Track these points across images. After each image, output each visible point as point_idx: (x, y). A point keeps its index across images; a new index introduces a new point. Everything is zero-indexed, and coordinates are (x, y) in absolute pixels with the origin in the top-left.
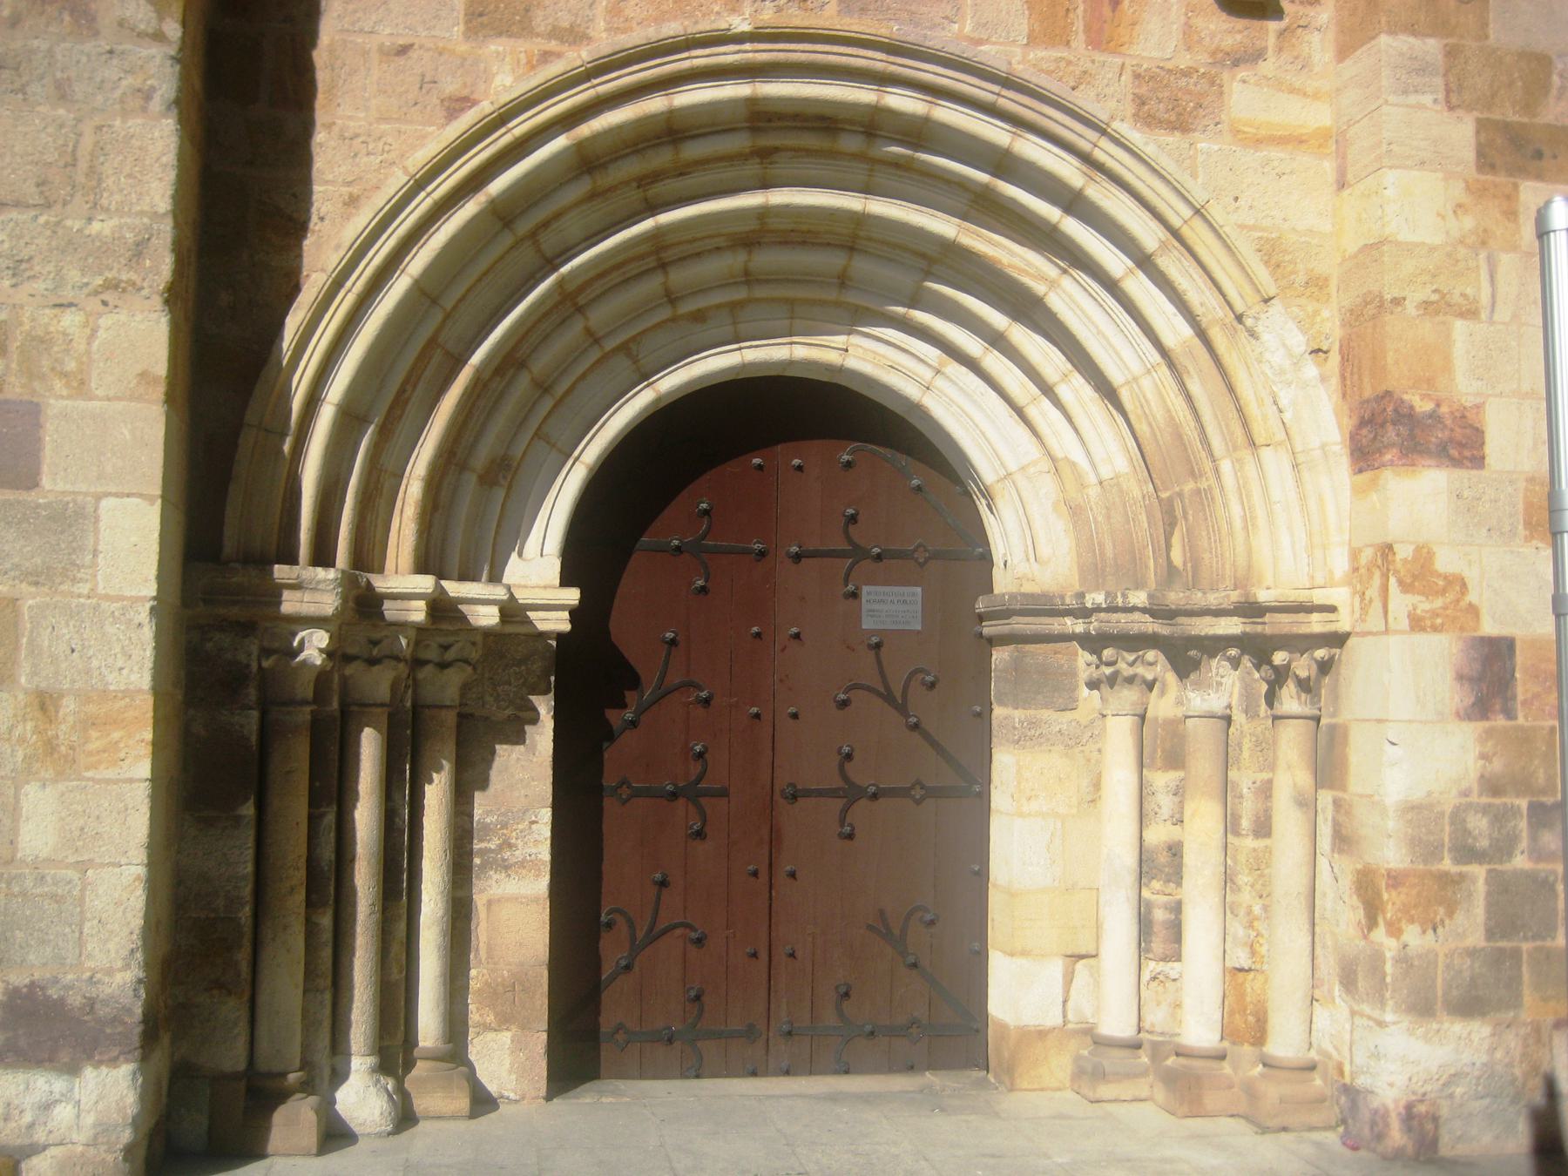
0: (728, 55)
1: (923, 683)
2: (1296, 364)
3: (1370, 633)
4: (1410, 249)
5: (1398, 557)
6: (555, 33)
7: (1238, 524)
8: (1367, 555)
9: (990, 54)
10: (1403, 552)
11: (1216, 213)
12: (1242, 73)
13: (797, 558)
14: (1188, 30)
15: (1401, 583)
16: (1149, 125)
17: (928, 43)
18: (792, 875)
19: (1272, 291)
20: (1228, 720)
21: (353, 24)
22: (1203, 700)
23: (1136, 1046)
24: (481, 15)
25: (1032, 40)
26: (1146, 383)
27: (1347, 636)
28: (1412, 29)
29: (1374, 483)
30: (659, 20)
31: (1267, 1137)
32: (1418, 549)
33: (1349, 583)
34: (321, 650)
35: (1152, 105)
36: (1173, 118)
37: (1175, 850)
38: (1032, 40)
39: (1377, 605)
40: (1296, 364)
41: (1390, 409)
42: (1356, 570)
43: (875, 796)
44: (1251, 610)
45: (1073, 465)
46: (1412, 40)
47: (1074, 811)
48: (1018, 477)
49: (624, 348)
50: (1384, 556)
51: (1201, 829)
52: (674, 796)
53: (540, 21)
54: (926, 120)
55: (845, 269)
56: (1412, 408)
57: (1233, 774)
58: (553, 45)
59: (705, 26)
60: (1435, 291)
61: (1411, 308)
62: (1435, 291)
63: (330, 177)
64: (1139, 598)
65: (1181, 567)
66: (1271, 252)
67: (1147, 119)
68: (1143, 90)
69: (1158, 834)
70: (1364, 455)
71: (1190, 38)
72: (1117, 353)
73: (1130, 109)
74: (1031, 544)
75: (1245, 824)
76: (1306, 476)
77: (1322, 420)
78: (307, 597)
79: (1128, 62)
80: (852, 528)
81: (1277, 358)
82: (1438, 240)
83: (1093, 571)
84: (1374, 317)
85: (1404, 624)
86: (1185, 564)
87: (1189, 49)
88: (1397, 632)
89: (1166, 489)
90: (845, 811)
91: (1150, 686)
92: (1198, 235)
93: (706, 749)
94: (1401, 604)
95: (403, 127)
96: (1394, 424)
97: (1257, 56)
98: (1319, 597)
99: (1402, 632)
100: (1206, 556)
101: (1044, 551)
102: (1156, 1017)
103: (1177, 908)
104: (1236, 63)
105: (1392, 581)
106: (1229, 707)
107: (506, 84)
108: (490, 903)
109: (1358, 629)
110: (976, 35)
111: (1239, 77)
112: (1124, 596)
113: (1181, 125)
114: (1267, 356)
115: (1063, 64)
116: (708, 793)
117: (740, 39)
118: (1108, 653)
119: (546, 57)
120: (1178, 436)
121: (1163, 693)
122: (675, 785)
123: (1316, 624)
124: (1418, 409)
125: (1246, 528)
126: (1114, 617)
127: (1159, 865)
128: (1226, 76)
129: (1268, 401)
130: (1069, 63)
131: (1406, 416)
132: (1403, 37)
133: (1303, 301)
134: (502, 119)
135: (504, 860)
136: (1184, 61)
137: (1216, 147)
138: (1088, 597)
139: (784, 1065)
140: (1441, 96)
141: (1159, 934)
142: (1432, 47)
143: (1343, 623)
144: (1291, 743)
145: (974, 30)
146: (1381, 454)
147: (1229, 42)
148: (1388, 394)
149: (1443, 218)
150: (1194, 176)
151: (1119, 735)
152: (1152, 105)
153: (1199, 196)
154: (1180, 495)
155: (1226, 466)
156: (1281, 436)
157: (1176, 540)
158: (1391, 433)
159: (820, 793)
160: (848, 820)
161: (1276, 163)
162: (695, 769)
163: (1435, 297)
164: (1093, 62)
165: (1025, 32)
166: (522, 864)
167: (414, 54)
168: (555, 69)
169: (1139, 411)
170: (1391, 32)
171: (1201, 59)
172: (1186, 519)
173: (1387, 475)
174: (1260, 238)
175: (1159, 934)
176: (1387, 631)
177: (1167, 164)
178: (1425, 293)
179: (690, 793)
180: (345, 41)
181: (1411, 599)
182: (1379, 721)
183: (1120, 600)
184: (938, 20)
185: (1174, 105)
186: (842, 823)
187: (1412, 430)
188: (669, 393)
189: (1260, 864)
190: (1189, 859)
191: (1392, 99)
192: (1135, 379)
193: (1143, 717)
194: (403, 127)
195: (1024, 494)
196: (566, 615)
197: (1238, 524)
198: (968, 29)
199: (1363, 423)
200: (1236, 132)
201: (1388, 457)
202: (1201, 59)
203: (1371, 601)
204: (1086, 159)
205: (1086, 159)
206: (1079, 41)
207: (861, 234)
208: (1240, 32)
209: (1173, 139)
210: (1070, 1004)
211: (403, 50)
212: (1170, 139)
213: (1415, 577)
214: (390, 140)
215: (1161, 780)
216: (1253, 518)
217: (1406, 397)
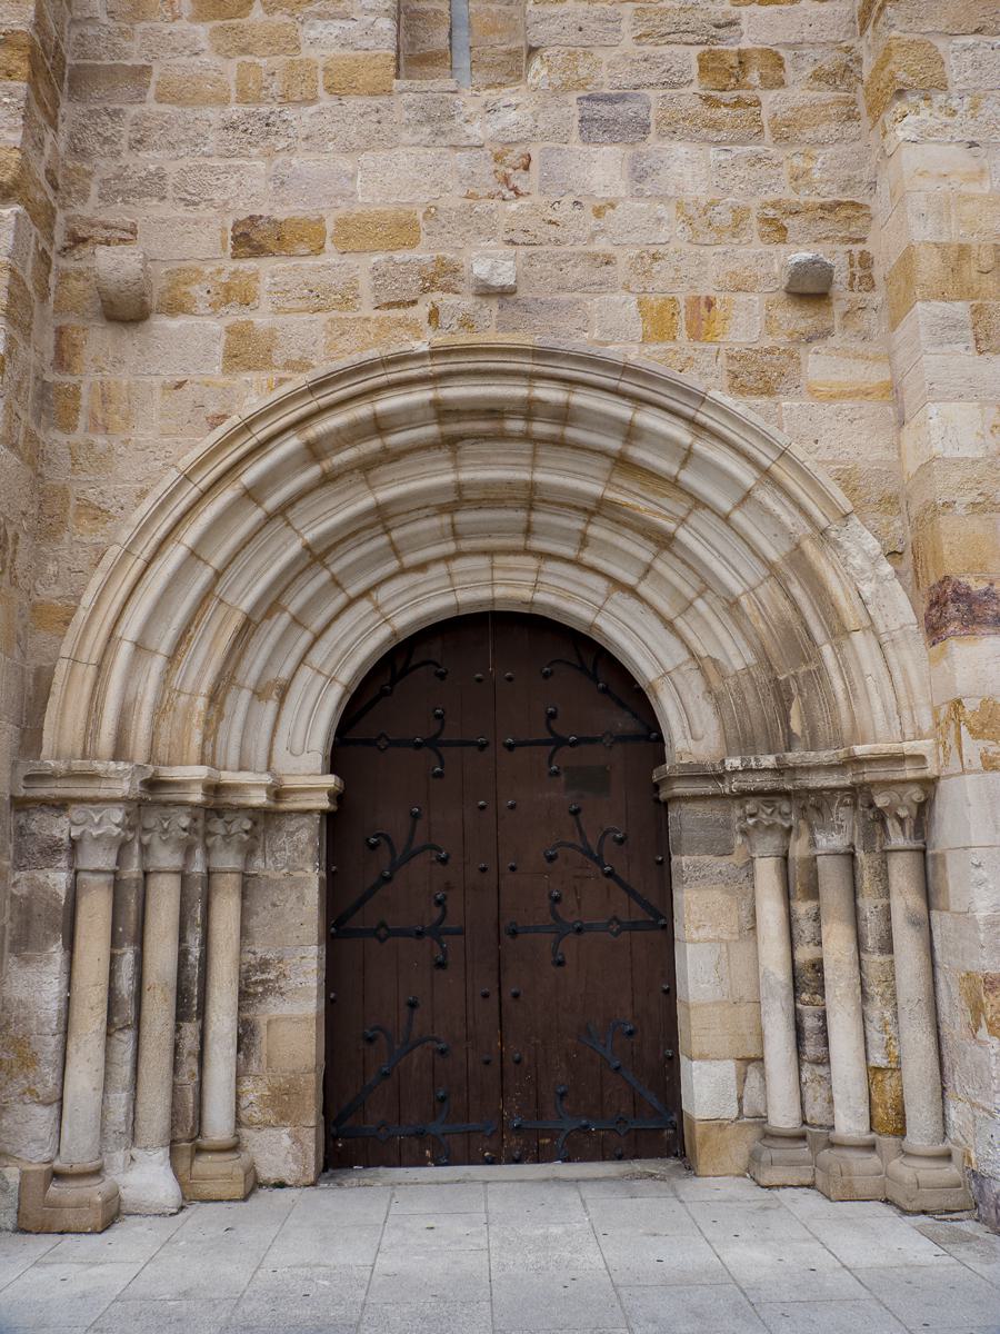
0: (413, 370)
1: (615, 839)
2: (874, 563)
3: (952, 775)
4: (956, 463)
6: (288, 365)
7: (841, 696)
9: (614, 352)
10: (970, 705)
11: (798, 451)
12: (815, 347)
14: (769, 319)
15: (971, 730)
16: (742, 393)
17: (562, 347)
19: (848, 507)
20: (852, 856)
22: (828, 841)
24: (236, 356)
25: (646, 339)
29: (944, 654)
30: (367, 346)
31: (906, 1218)
32: (985, 702)
33: (935, 737)
35: (744, 378)
37: (818, 966)
38: (646, 339)
39: (955, 750)
43: (579, 930)
44: (855, 762)
47: (737, 937)
48: (674, 675)
49: (365, 594)
50: (956, 709)
51: (837, 945)
53: (278, 357)
54: (567, 405)
55: (581, 550)
56: (968, 588)
57: (860, 902)
58: (286, 374)
61: (960, 510)
64: (769, 761)
65: (799, 734)
67: (740, 389)
69: (805, 954)
70: (934, 631)
71: (770, 325)
72: (737, 571)
73: (725, 380)
74: (692, 731)
76: (890, 652)
77: (900, 610)
78: (104, 784)
79: (722, 347)
80: (552, 723)
82: (980, 454)
83: (743, 742)
85: (978, 764)
86: (802, 731)
87: (771, 333)
88: (971, 772)
90: (557, 943)
92: (783, 472)
93: (445, 897)
94: (972, 748)
95: (180, 439)
96: (953, 601)
98: (908, 747)
99: (976, 771)
100: (821, 724)
101: (699, 730)
102: (815, 1111)
103: (823, 1017)
104: (809, 340)
106: (852, 845)
107: (254, 403)
108: (269, 1022)
109: (944, 774)
110: (602, 339)
113: (768, 390)
114: (850, 560)
115: (671, 354)
116: (448, 932)
117: (420, 357)
118: (749, 807)
119: (281, 381)
120: (789, 631)
121: (798, 837)
123: (909, 772)
124: (974, 589)
125: (848, 698)
126: (750, 777)
127: (806, 980)
129: (854, 595)
130: (676, 353)
131: (963, 596)
132: (935, 303)
134: (247, 427)
136: (768, 343)
137: (797, 404)
138: (727, 762)
139: (619, 1152)
140: (972, 344)
141: (809, 1042)
142: (961, 309)
143: (931, 770)
144: (902, 873)
146: (947, 627)
147: (803, 325)
148: (947, 578)
149: (983, 437)
150: (780, 428)
151: (767, 870)
152: (744, 378)
153: (782, 439)
154: (795, 677)
155: (827, 650)
157: (794, 712)
158: (951, 609)
159: (536, 930)
162: (437, 912)
163: (981, 499)
164: (695, 350)
165: (640, 334)
167: (186, 387)
169: (756, 613)
170: (925, 300)
171: (780, 340)
172: (801, 696)
173: (952, 642)
175: (809, 1042)
176: (963, 772)
177: (755, 419)
178: (972, 497)
180: (138, 382)
181: (982, 744)
182: (966, 848)
183: (753, 763)
184: (572, 331)
185: (761, 376)
186: (555, 955)
187: (970, 606)
188: (404, 629)
189: (890, 978)
191: (933, 350)
192: (753, 590)
193: (786, 858)
194: (180, 439)
195: (680, 688)
196: (325, 796)
197: (841, 696)
199: (933, 604)
202: (780, 340)
204: (691, 421)
205: (691, 421)
206: (683, 336)
208: (811, 317)
209: (762, 401)
211: (179, 385)
213: (984, 726)
215: (803, 908)
216: (854, 690)
217: (961, 580)
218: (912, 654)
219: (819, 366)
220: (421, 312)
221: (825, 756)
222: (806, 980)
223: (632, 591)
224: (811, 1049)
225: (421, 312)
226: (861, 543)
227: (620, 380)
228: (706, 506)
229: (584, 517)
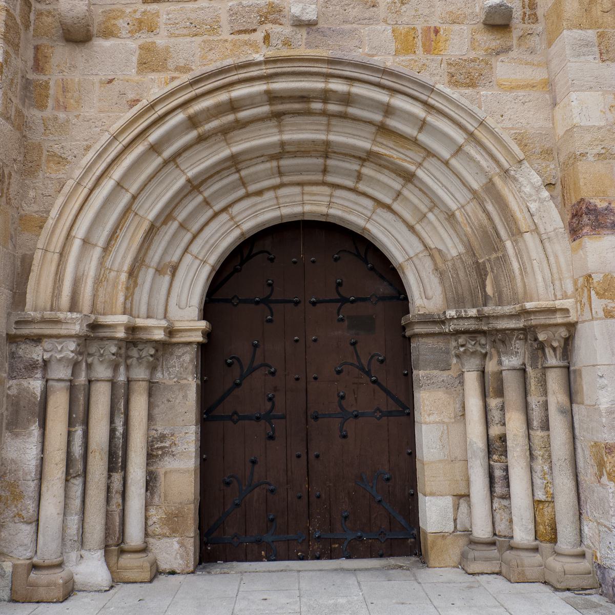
0: (254, 72)
1: (378, 360)
2: (538, 190)
4: (588, 129)
5: (594, 281)
6: (177, 69)
7: (517, 272)
8: (581, 280)
9: (378, 60)
10: (597, 278)
11: (491, 122)
12: (501, 58)
13: (314, 304)
15: (597, 293)
16: (456, 86)
17: (345, 58)
18: (317, 457)
19: (522, 156)
21: (89, 72)
22: (509, 361)
23: (493, 544)
24: (145, 63)
25: (397, 53)
26: (468, 208)
27: (577, 323)
28: (580, 27)
29: (580, 246)
30: (226, 57)
32: (606, 276)
34: (72, 352)
35: (457, 77)
36: (468, 81)
37: (503, 438)
38: (397, 53)
39: (587, 306)
40: (538, 190)
41: (584, 207)
42: (577, 290)
43: (356, 416)
44: (526, 313)
45: (440, 251)
46: (580, 31)
48: (415, 259)
49: (224, 209)
50: (588, 281)
51: (515, 425)
52: (258, 419)
53: (171, 64)
54: (349, 94)
56: (596, 206)
57: (529, 399)
58: (176, 74)
59: (243, 59)
60: (603, 148)
61: (591, 158)
62: (603, 148)
63: (78, 138)
64: (473, 312)
65: (492, 296)
66: (521, 140)
67: (454, 82)
68: (453, 70)
69: (495, 431)
70: (575, 232)
73: (446, 78)
74: (425, 294)
75: (535, 424)
76: (547, 244)
77: (553, 220)
80: (340, 289)
81: (528, 189)
84: (573, 164)
85: (601, 314)
88: (597, 319)
89: (482, 258)
90: (342, 424)
91: (485, 355)
92: (481, 135)
93: (274, 396)
95: (111, 114)
97: (508, 49)
98: (559, 304)
99: (600, 319)
100: (505, 289)
101: (430, 293)
103: (506, 469)
104: (498, 54)
105: (593, 292)
106: (524, 364)
107: (156, 92)
108: (166, 473)
109: (580, 320)
110: (369, 53)
111: (500, 60)
112: (465, 311)
113: (472, 84)
114: (523, 188)
115: (413, 62)
117: (258, 64)
119: (173, 79)
122: (260, 414)
123: (559, 319)
124: (599, 206)
125: (521, 274)
126: (461, 322)
127: (496, 447)
128: (493, 60)
129: (525, 210)
130: (416, 61)
131: (592, 210)
132: (575, 30)
133: (539, 161)
134: (152, 107)
135: (173, 452)
136: (472, 55)
137: (490, 93)
140: (598, 56)
141: (499, 485)
142: (591, 34)
143: (573, 318)
144: (555, 381)
145: (369, 51)
146: (582, 230)
148: (582, 200)
150: (480, 107)
151: (471, 380)
153: (481, 114)
155: (508, 244)
156: (533, 227)
157: (488, 282)
158: (585, 219)
160: (344, 428)
161: (521, 98)
163: (603, 151)
164: (427, 59)
165: (394, 49)
166: (182, 453)
168: (176, 83)
169: (465, 222)
170: (569, 29)
172: (493, 272)
174: (516, 133)
175: (499, 485)
176: (592, 319)
178: (598, 149)
179: (268, 417)
180: (85, 79)
181: (604, 302)
182: (594, 366)
183: (463, 314)
184: (352, 48)
185: (468, 76)
186: (341, 431)
187: (596, 217)
189: (547, 446)
190: (510, 443)
192: (463, 207)
193: (483, 372)
194: (111, 114)
195: (418, 267)
197: (517, 272)
198: (366, 50)
199: (574, 216)
200: (500, 85)
201: (585, 231)
202: (480, 53)
203: (584, 304)
204: (425, 103)
205: (425, 103)
206: (420, 51)
207: (330, 150)
208: (499, 39)
209: (469, 91)
210: (458, 521)
211: (110, 81)
212: (467, 91)
214: (104, 120)
215: (494, 402)
217: (591, 201)
218: (561, 246)
219: (505, 69)
220: (259, 36)
221: (507, 309)
222: (496, 447)
223: (389, 208)
224: (499, 490)
225: (259, 36)
226: (530, 178)
227: (381, 78)
228: (434, 156)
229: (360, 162)
